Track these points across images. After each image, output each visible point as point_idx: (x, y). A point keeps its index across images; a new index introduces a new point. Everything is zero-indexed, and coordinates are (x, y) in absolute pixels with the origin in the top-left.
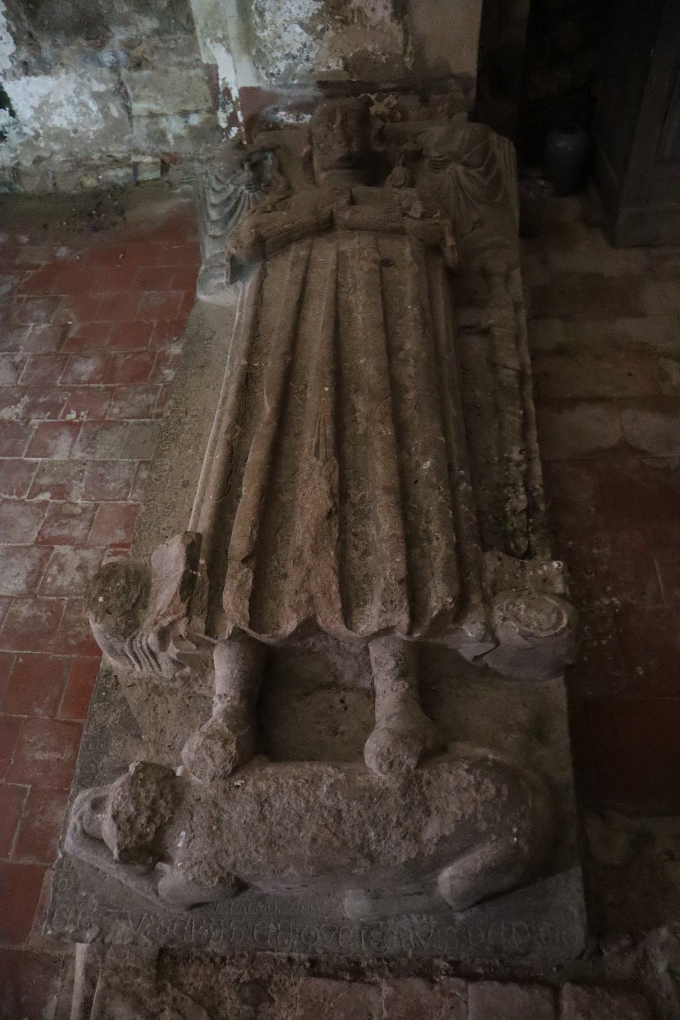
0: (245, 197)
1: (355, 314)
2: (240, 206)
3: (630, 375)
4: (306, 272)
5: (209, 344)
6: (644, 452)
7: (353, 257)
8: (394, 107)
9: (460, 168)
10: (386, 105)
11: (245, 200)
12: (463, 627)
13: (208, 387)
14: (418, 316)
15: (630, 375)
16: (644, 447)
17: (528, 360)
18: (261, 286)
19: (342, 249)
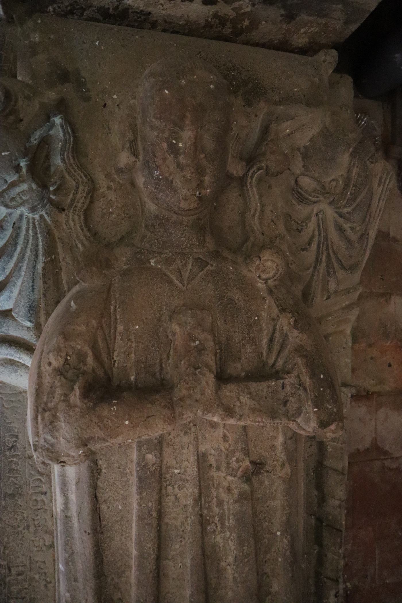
0: (28, 222)
1: (223, 564)
2: (21, 241)
3: (390, 365)
4: (160, 502)
5: (13, 456)
6: (386, 453)
7: (218, 469)
8: (245, 13)
9: (330, 213)
10: (233, 9)
11: (27, 230)
12: (122, 166)
13: (28, 527)
14: (288, 553)
15: (390, 365)
16: (387, 448)
17: (347, 465)
18: (96, 497)
19: (203, 448)
